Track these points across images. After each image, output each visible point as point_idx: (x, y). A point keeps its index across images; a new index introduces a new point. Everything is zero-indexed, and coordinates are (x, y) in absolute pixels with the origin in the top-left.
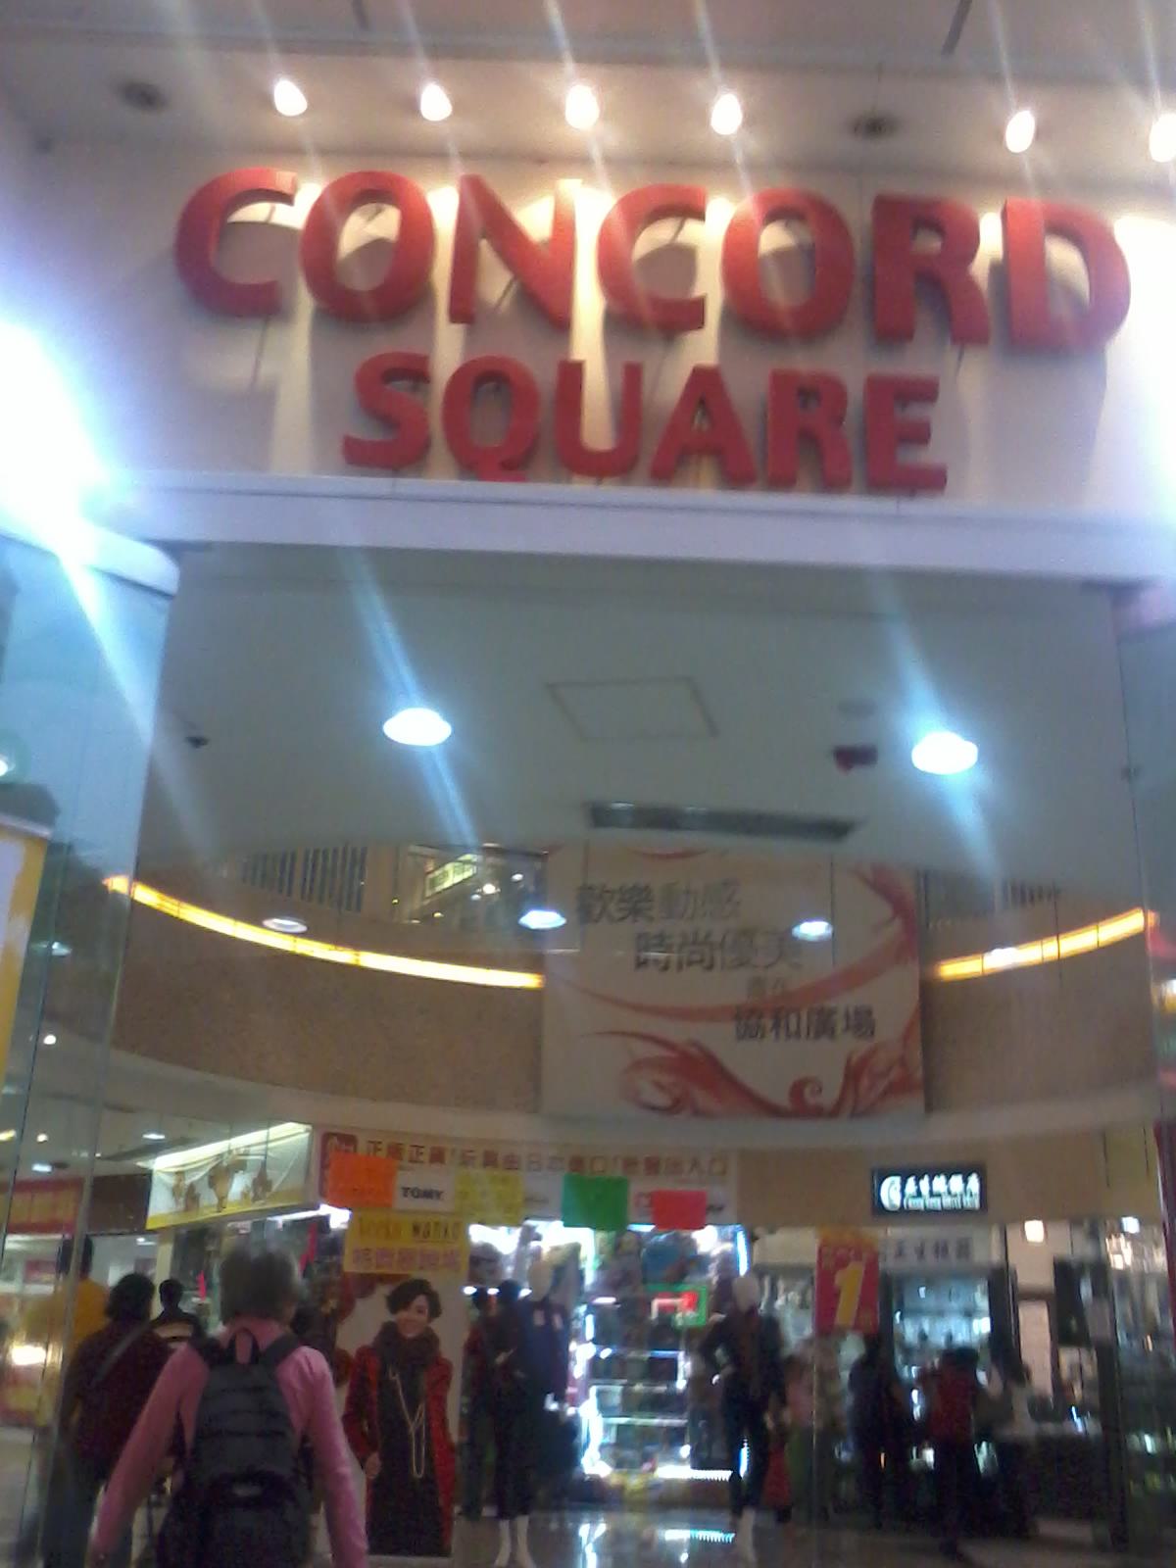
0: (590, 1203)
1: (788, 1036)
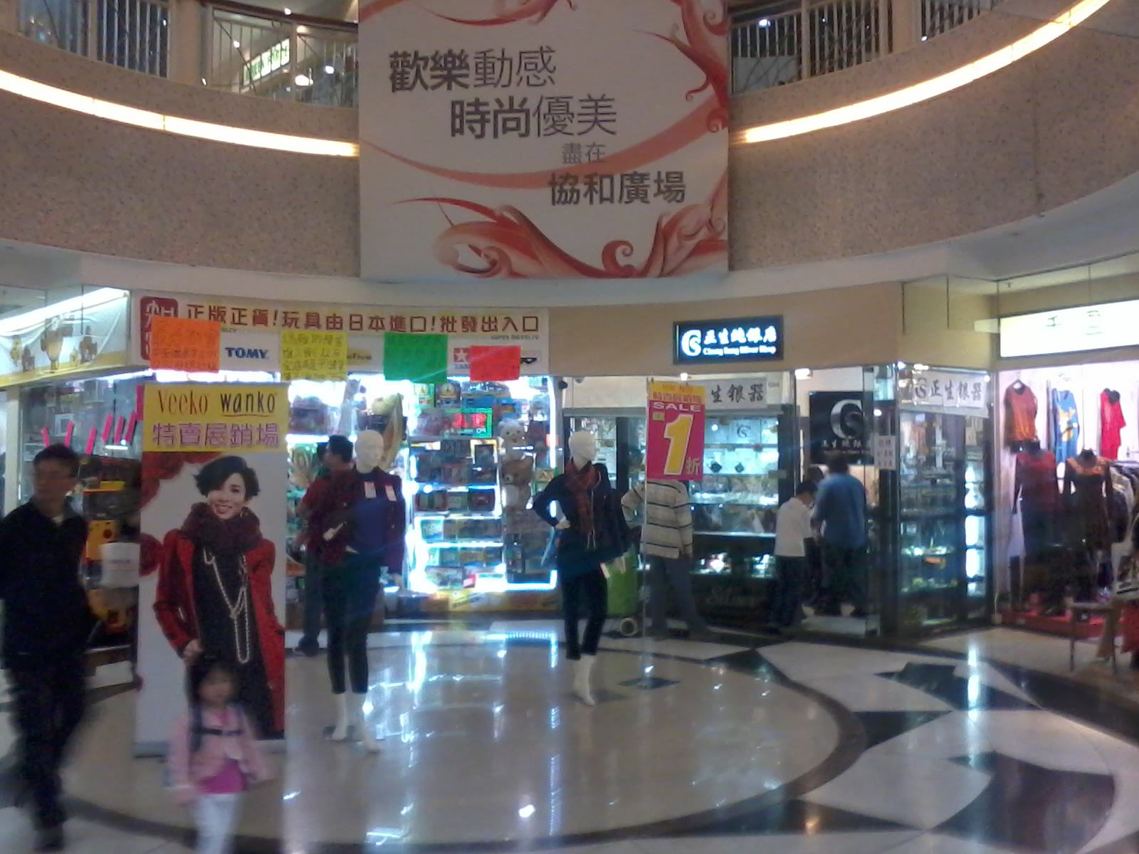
0: (407, 349)
1: (602, 200)
